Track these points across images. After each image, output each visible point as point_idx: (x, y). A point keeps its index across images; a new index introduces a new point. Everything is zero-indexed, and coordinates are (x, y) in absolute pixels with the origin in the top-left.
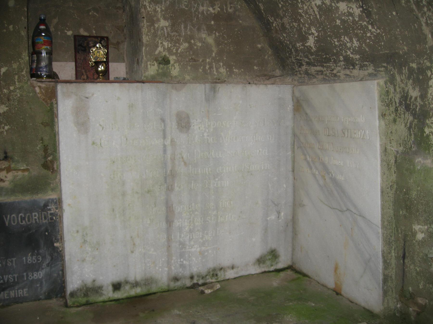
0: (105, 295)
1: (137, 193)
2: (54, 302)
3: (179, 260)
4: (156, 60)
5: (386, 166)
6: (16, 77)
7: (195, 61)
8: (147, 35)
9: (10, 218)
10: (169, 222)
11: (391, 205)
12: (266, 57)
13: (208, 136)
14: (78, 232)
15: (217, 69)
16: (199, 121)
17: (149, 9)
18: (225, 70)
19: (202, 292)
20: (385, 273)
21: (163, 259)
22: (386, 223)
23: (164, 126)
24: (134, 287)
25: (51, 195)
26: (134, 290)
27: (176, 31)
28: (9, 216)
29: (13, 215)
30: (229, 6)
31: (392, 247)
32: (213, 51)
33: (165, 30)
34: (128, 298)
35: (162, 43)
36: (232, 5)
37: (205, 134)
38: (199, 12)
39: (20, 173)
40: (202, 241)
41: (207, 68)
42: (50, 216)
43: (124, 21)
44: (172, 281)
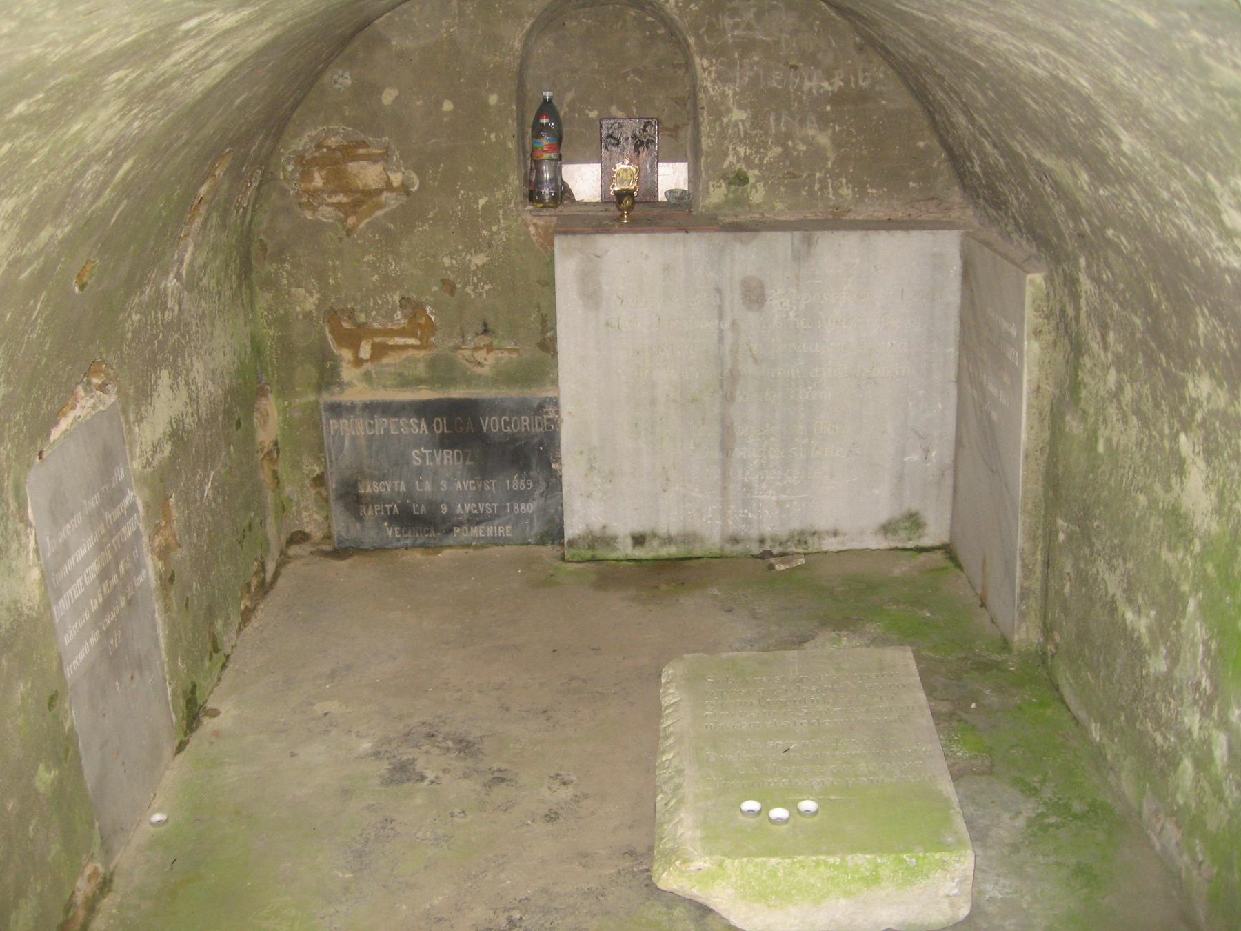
0: (620, 550)
1: (675, 401)
2: (548, 551)
3: (741, 512)
4: (724, 177)
5: (1037, 414)
6: (501, 212)
7: (794, 176)
8: (709, 136)
9: (489, 421)
10: (726, 448)
11: (1041, 478)
12: (935, 164)
13: (796, 316)
14: (581, 453)
15: (835, 190)
16: (780, 291)
17: (712, 93)
18: (850, 191)
19: (771, 567)
20: (1025, 585)
21: (714, 507)
22: (1030, 506)
23: (721, 300)
24: (665, 543)
25: (549, 390)
26: (665, 549)
27: (761, 128)
28: (487, 419)
29: (493, 418)
30: (860, 76)
31: (1038, 546)
32: (827, 159)
33: (741, 127)
34: (655, 560)
35: (734, 149)
36: (866, 74)
37: (792, 314)
38: (802, 92)
39: (506, 354)
40: (781, 485)
41: (816, 189)
42: (546, 423)
43: (688, 89)
44: (728, 543)
